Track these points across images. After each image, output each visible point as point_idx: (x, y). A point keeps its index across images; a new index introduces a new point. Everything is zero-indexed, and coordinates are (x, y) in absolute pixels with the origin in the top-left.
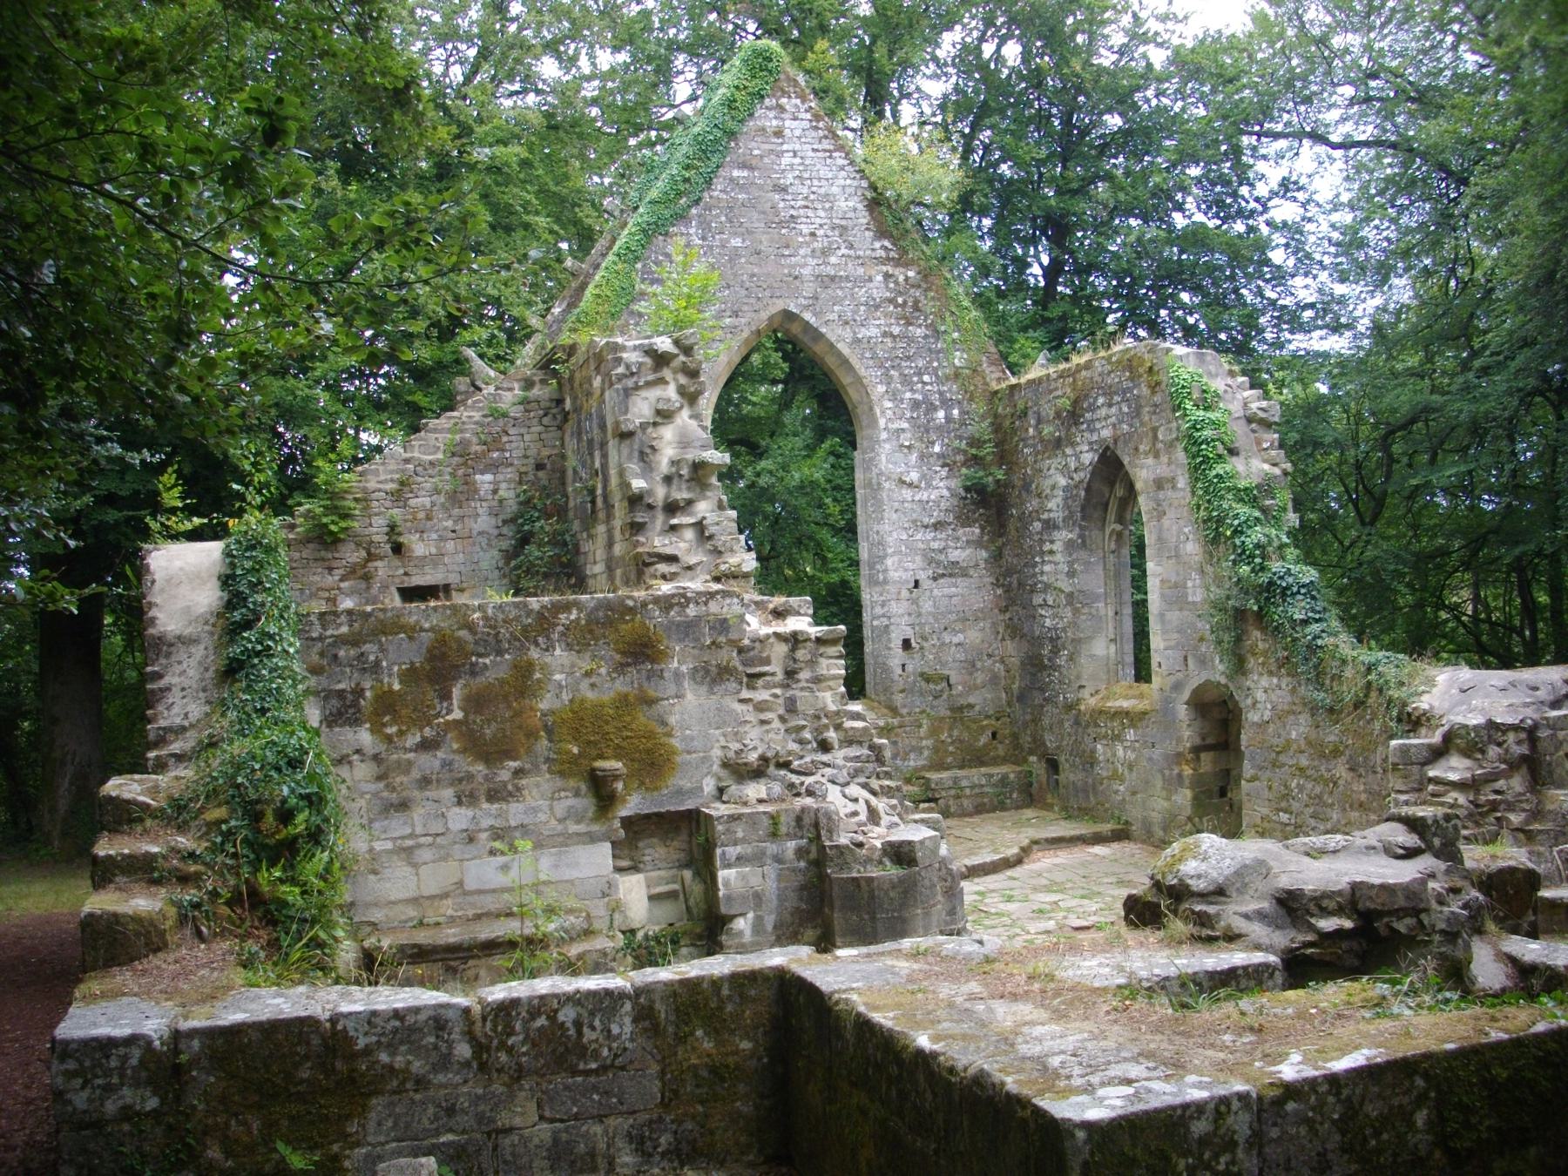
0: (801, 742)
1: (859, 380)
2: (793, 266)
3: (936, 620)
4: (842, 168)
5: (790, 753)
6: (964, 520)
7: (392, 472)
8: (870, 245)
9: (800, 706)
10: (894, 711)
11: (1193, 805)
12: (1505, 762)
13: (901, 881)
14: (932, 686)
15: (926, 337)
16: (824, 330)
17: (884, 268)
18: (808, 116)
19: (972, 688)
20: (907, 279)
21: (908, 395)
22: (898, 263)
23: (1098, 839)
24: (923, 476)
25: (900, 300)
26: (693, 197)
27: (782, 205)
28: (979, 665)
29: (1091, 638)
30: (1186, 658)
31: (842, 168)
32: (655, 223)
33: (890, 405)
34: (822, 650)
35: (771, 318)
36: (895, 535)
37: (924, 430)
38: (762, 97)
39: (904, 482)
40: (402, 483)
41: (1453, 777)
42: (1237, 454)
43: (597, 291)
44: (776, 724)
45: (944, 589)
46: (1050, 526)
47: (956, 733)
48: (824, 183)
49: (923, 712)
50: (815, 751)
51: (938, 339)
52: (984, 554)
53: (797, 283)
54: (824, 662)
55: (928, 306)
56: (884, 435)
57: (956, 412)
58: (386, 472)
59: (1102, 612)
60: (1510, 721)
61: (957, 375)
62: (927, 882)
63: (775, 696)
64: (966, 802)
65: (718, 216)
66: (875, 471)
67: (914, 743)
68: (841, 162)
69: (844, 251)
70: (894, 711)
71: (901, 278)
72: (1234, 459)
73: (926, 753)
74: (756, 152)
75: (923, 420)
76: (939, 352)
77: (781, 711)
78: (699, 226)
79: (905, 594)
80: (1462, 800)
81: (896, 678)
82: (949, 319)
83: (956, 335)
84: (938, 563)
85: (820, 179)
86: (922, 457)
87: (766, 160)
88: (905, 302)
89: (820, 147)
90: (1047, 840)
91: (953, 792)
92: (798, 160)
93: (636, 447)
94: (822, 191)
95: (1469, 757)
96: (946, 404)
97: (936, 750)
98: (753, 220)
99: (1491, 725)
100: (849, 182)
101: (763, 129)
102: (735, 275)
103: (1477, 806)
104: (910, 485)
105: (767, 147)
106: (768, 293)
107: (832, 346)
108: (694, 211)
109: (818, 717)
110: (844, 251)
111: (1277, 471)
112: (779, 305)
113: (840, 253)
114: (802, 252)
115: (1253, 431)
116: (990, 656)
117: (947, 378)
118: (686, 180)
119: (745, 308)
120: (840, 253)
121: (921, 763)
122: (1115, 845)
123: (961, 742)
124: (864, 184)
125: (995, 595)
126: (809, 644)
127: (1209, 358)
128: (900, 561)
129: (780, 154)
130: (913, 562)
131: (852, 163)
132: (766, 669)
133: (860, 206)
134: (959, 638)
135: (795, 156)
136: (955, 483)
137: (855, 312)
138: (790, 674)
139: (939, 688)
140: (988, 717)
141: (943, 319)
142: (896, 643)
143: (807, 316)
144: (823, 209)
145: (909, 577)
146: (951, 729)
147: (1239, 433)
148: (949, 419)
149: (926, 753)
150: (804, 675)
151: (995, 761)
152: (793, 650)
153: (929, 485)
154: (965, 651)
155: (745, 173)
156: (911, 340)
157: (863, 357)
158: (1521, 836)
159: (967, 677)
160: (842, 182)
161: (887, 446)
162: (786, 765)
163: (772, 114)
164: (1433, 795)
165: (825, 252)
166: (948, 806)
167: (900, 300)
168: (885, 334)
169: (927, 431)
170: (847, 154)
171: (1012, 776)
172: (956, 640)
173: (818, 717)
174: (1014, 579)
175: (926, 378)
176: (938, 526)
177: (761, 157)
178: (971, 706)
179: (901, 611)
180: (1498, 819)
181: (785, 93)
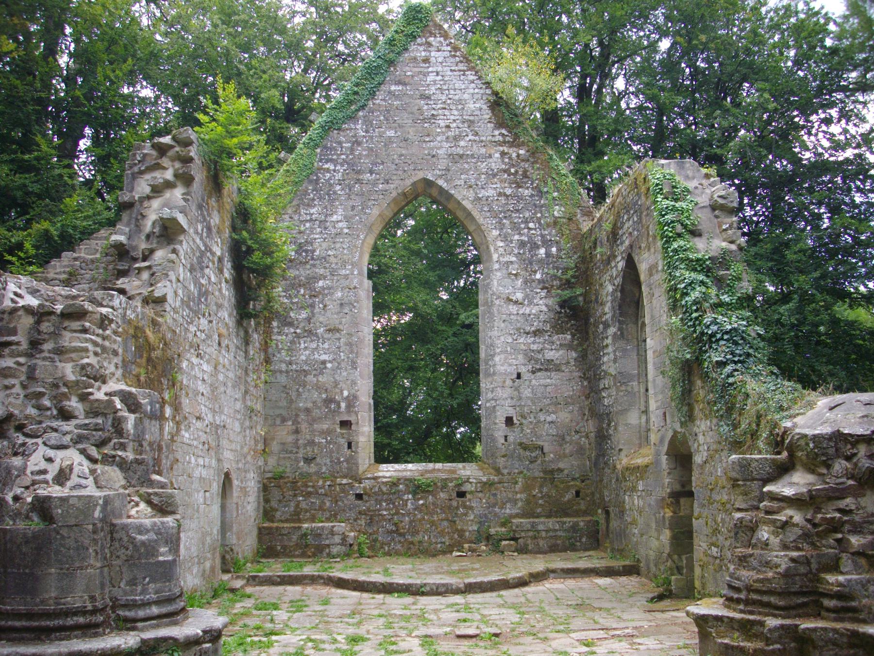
0: (39, 407)
1: (479, 226)
2: (432, 149)
3: (534, 403)
4: (473, 82)
5: (27, 417)
6: (558, 327)
7: (65, 266)
8: (490, 132)
9: (38, 373)
10: (498, 471)
11: (672, 544)
12: (852, 477)
13: (35, 536)
14: (528, 453)
15: (532, 196)
16: (453, 192)
17: (501, 149)
18: (449, 48)
19: (561, 457)
20: (518, 156)
21: (516, 237)
22: (512, 145)
23: (609, 572)
24: (526, 296)
25: (513, 170)
26: (359, 104)
27: (426, 107)
28: (568, 438)
29: (626, 410)
30: (665, 414)
31: (473, 82)
32: (331, 122)
33: (501, 244)
34: (66, 324)
35: (414, 184)
36: (502, 339)
37: (528, 263)
38: (415, 37)
39: (511, 300)
40: (70, 274)
41: (788, 492)
42: (700, 235)
43: (288, 168)
44: (18, 389)
45: (542, 380)
46: (606, 326)
47: (545, 490)
48: (458, 92)
49: (521, 472)
50: (55, 418)
51: (541, 197)
52: (574, 355)
53: (434, 160)
54: (67, 335)
55: (535, 174)
56: (496, 266)
57: (554, 250)
58: (61, 266)
59: (636, 390)
60: (860, 431)
61: (555, 223)
62: (71, 543)
63: (19, 364)
64: (541, 543)
65: (378, 116)
66: (490, 292)
67: (510, 495)
68: (472, 78)
69: (471, 137)
70: (498, 471)
71: (514, 155)
72: (696, 239)
73: (520, 504)
74: (409, 73)
75: (528, 255)
76: (542, 206)
77: (23, 378)
78: (364, 123)
79: (509, 383)
80: (798, 517)
81: (500, 446)
82: (550, 183)
83: (555, 194)
84: (537, 361)
85: (455, 89)
86: (526, 282)
87: (416, 78)
88: (517, 172)
89: (456, 68)
90: (563, 570)
91: (531, 534)
92: (440, 78)
93: (134, 216)
94: (457, 97)
95: (812, 471)
96: (546, 243)
97: (528, 502)
98: (405, 119)
99: (838, 437)
100: (476, 91)
101: (415, 58)
102: (388, 155)
103: (815, 525)
104: (516, 302)
105: (417, 70)
106: (412, 167)
107: (459, 203)
108: (361, 113)
109: (56, 386)
110: (471, 137)
111: (733, 247)
112: (420, 175)
113: (467, 139)
114: (439, 139)
115: (717, 217)
116: (577, 432)
117: (548, 225)
118: (356, 93)
119: (395, 178)
120: (467, 139)
121: (515, 511)
122: (623, 579)
123: (549, 497)
124: (489, 91)
125: (582, 386)
126: (53, 317)
127: (688, 165)
128: (506, 359)
129: (426, 74)
130: (516, 359)
131: (480, 78)
132: (13, 338)
133: (485, 107)
134: (552, 417)
135: (437, 75)
136: (550, 302)
137: (478, 179)
138: (35, 344)
139: (533, 455)
140: (574, 479)
141: (546, 183)
142: (500, 419)
143: (440, 182)
144: (457, 109)
145: (513, 370)
146: (541, 486)
147: (703, 219)
148: (548, 254)
149: (520, 504)
150: (48, 346)
151: (577, 514)
152: (38, 322)
153: (531, 303)
154: (557, 427)
155: (400, 88)
156: (520, 198)
157: (482, 210)
158: (863, 561)
159: (557, 448)
160: (472, 91)
161: (499, 274)
162: (20, 428)
163: (421, 48)
164: (768, 512)
165: (457, 138)
166: (526, 545)
167: (513, 170)
168: (500, 194)
169: (531, 264)
170: (476, 72)
171: (582, 524)
172: (549, 419)
173: (56, 386)
174: (591, 373)
175: (531, 225)
176: (537, 333)
177: (413, 76)
178: (560, 470)
179: (505, 396)
180: (838, 541)
181: (432, 34)
